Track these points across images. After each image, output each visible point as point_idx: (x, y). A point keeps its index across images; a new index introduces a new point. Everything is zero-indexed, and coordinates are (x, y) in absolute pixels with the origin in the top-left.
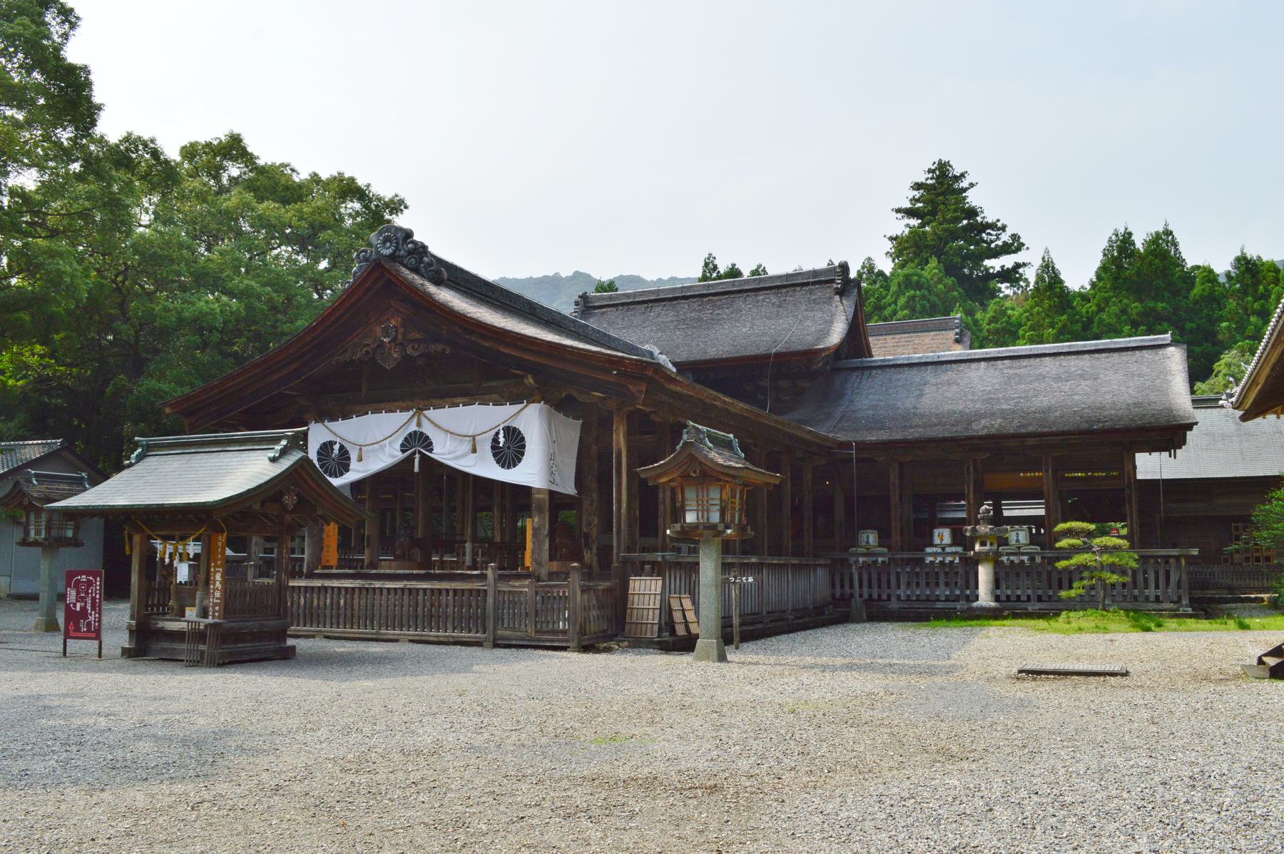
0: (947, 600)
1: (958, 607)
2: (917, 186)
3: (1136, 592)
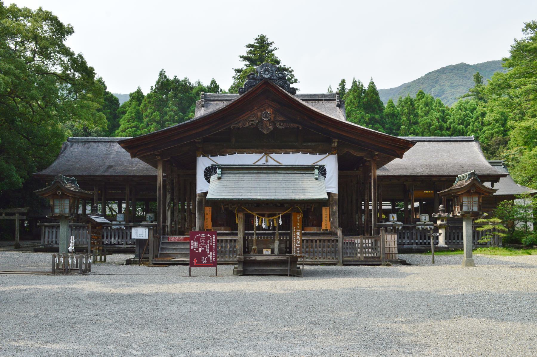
0: (408, 245)
1: (413, 247)
3: (454, 241)
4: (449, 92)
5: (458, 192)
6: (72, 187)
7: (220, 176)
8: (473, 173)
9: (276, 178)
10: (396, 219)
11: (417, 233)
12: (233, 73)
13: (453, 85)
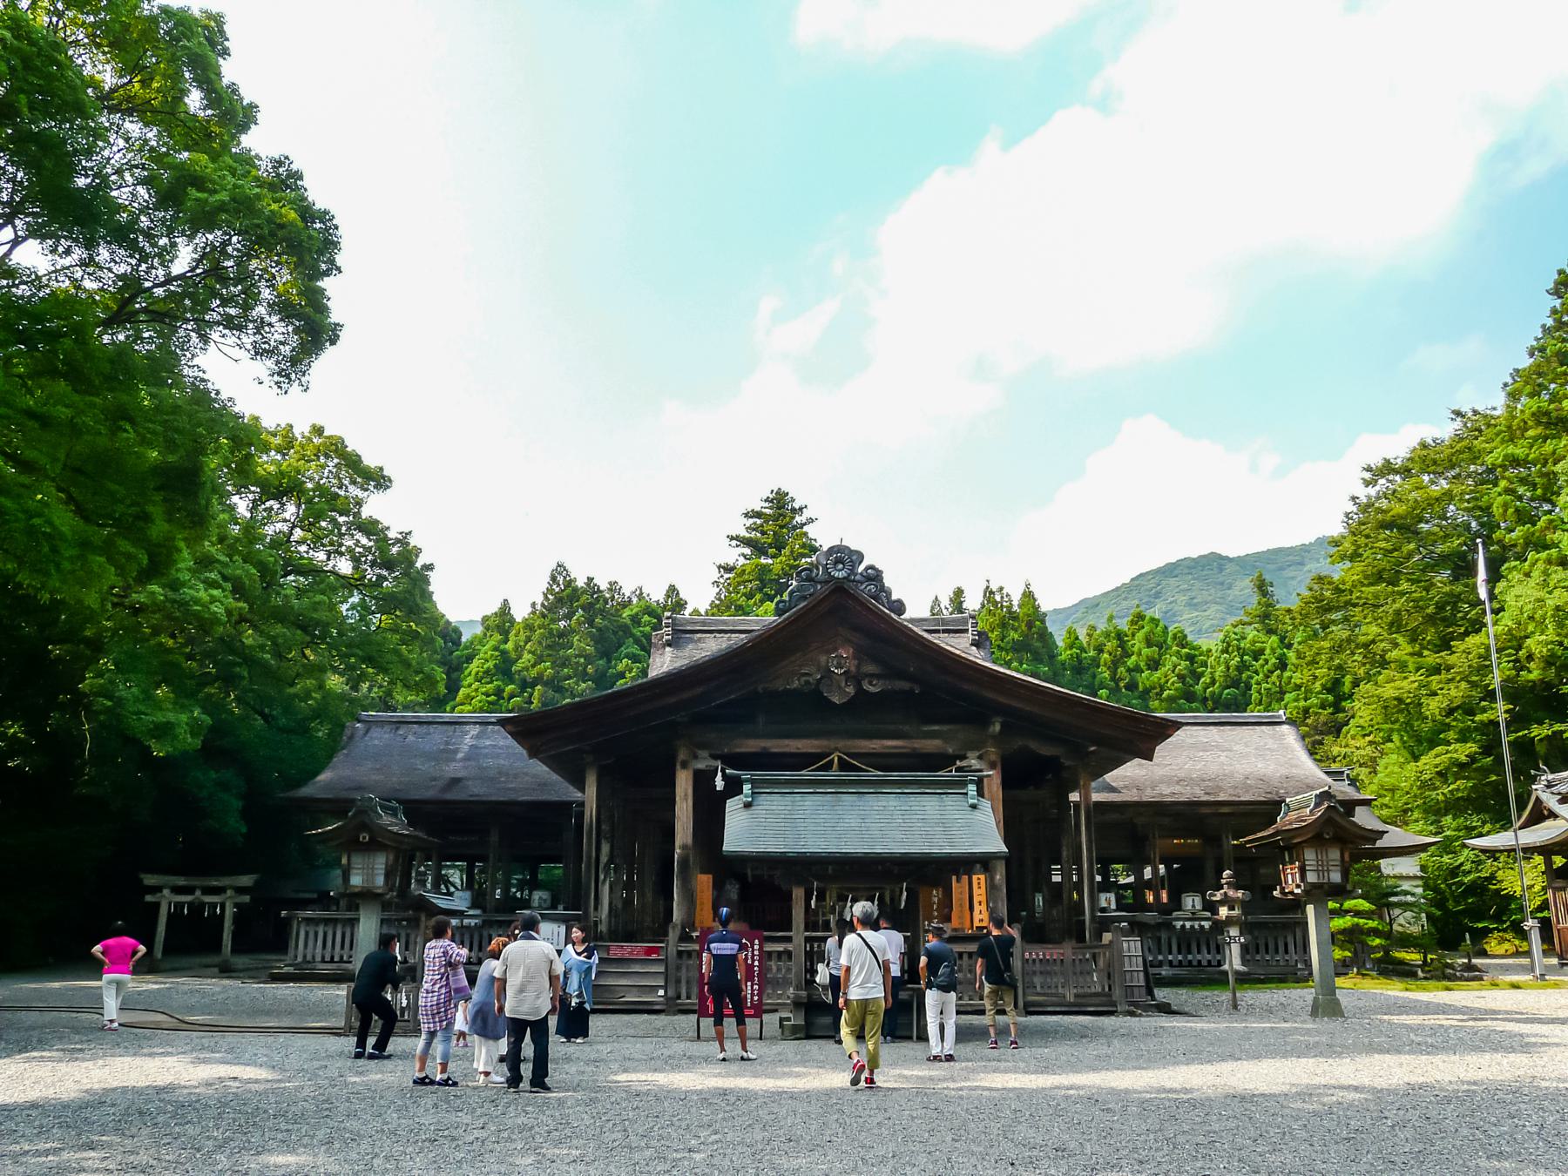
1: (1163, 973)
2: (1028, 596)
3: (1258, 957)
4: (1185, 617)
5: (1294, 837)
6: (394, 823)
7: (750, 799)
8: (1326, 792)
9: (880, 803)
10: (1199, 907)
11: (1170, 939)
12: (715, 575)
13: (1195, 601)
